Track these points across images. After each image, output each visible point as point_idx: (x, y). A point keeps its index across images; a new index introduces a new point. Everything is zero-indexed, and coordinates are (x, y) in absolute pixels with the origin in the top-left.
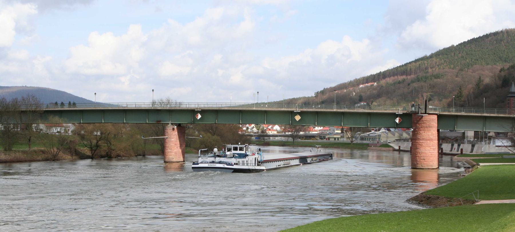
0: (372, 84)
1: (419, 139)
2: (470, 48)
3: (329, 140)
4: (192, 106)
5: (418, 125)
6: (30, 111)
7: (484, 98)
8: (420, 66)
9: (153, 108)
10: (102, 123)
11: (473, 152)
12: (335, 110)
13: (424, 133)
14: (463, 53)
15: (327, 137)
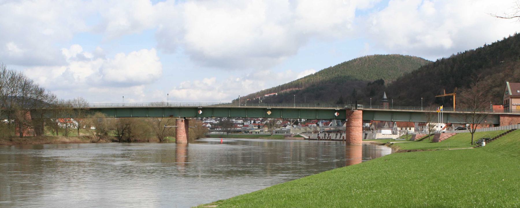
0: (274, 94)
1: (351, 126)
2: (343, 68)
3: (252, 133)
4: (197, 105)
5: (350, 117)
6: (79, 109)
7: (508, 83)
8: (308, 81)
9: (168, 107)
10: (131, 117)
11: (367, 138)
12: (294, 107)
13: (355, 122)
14: (338, 72)
15: (250, 131)
